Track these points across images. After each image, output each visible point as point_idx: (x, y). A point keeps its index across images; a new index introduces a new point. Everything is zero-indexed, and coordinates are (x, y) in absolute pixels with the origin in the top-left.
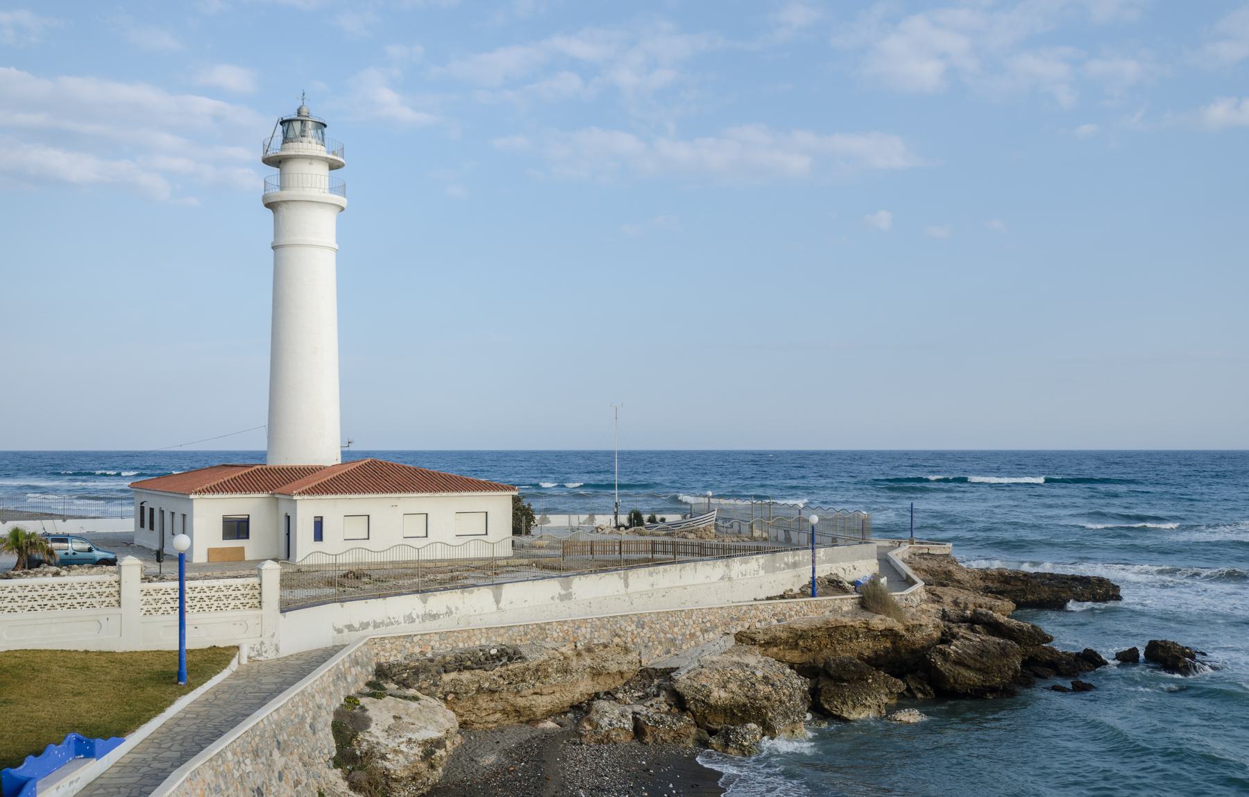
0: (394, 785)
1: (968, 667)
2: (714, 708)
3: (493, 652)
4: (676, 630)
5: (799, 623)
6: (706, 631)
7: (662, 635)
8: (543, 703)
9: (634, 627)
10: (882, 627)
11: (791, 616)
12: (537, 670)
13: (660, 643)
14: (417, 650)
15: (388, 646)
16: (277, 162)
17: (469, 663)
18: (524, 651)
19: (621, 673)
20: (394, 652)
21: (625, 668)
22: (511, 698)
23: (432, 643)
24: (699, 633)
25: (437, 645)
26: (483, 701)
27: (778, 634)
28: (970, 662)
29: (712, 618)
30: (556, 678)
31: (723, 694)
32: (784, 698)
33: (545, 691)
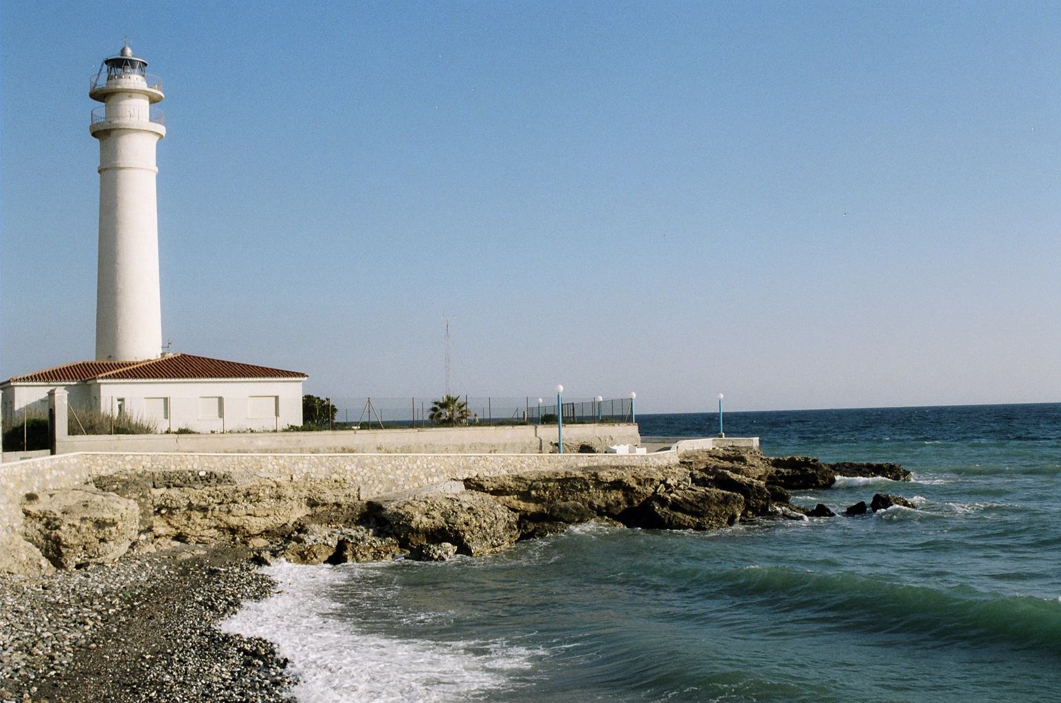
0: (64, 551)
1: (684, 511)
2: (416, 531)
3: (202, 474)
4: (398, 472)
5: (821, 617)
6: (431, 475)
7: (383, 475)
8: (257, 524)
9: (354, 466)
10: (611, 479)
11: (521, 468)
12: (248, 494)
13: (380, 482)
14: (129, 467)
15: (100, 461)
16: (101, 96)
17: (178, 482)
18: (235, 477)
19: (338, 505)
20: (106, 467)
21: (342, 500)
22: (224, 517)
23: (144, 463)
24: (422, 477)
25: (149, 465)
26: (197, 516)
27: (507, 482)
28: (688, 507)
29: (438, 465)
30: (268, 503)
31: (425, 519)
32: (484, 525)
33: (258, 513)
